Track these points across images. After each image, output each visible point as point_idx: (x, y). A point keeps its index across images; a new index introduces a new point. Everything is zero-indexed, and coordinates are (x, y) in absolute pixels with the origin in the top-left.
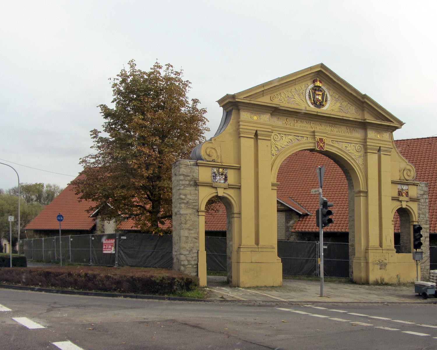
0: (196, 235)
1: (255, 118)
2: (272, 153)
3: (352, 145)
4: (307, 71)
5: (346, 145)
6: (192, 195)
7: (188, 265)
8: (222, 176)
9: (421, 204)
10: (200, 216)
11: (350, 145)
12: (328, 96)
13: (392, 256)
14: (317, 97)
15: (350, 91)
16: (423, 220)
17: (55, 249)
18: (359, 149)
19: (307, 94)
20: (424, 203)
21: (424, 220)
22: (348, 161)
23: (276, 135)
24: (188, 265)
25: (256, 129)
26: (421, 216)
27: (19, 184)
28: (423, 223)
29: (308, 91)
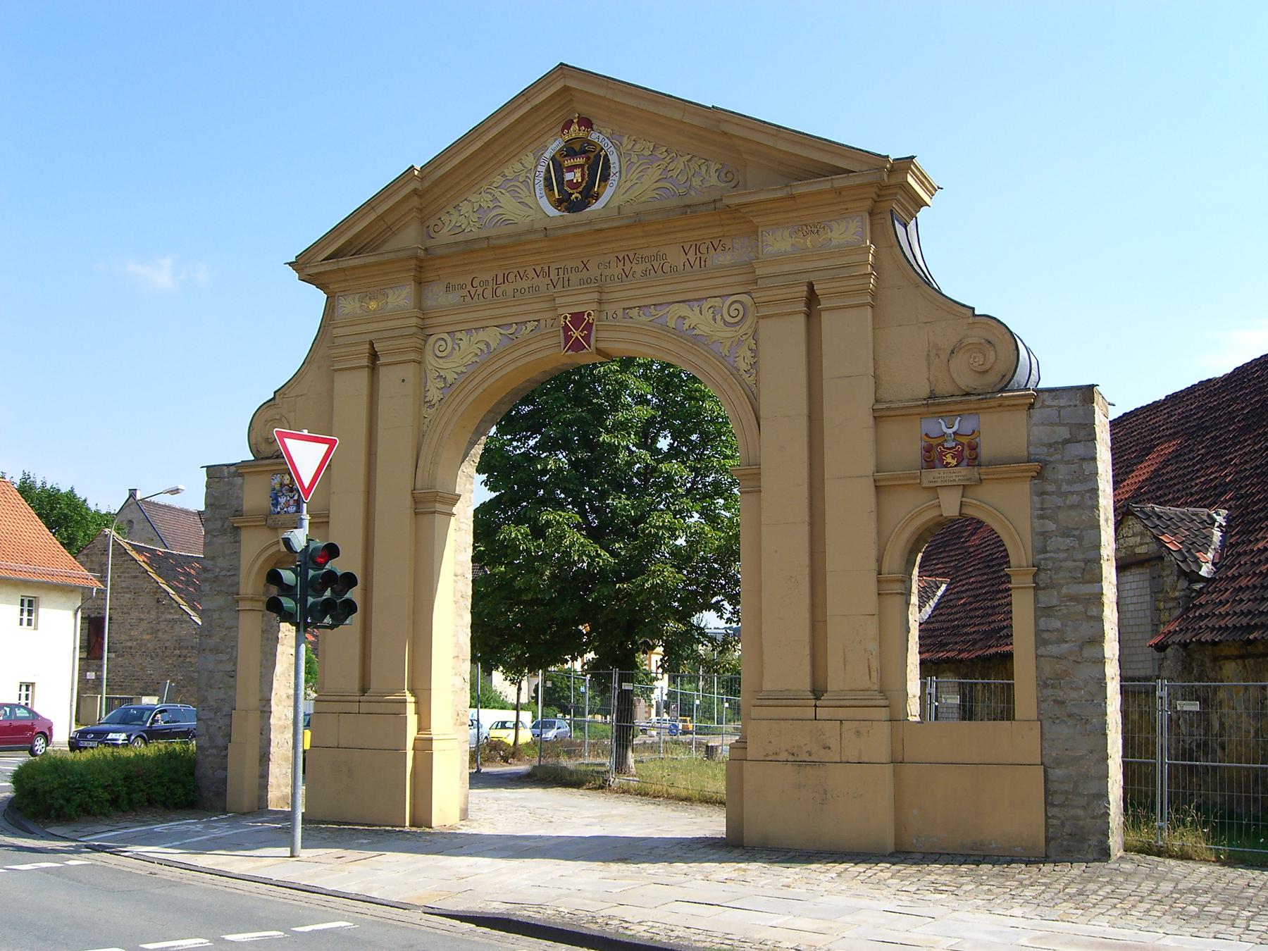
0: (229, 667)
1: (373, 305)
2: (427, 399)
3: (706, 305)
4: (515, 110)
5: (683, 310)
6: (227, 558)
7: (210, 748)
8: (291, 495)
9: (1050, 488)
10: (241, 613)
11: (697, 310)
12: (613, 159)
13: (770, 742)
14: (568, 176)
15: (479, 144)
16: (1065, 560)
17: (716, 695)
18: (734, 313)
19: (540, 180)
20: (1069, 482)
21: (1070, 564)
22: (486, 385)
23: (442, 339)
24: (210, 748)
25: (367, 338)
26: (1054, 543)
27: (960, 514)
28: (1062, 574)
29: (542, 169)
